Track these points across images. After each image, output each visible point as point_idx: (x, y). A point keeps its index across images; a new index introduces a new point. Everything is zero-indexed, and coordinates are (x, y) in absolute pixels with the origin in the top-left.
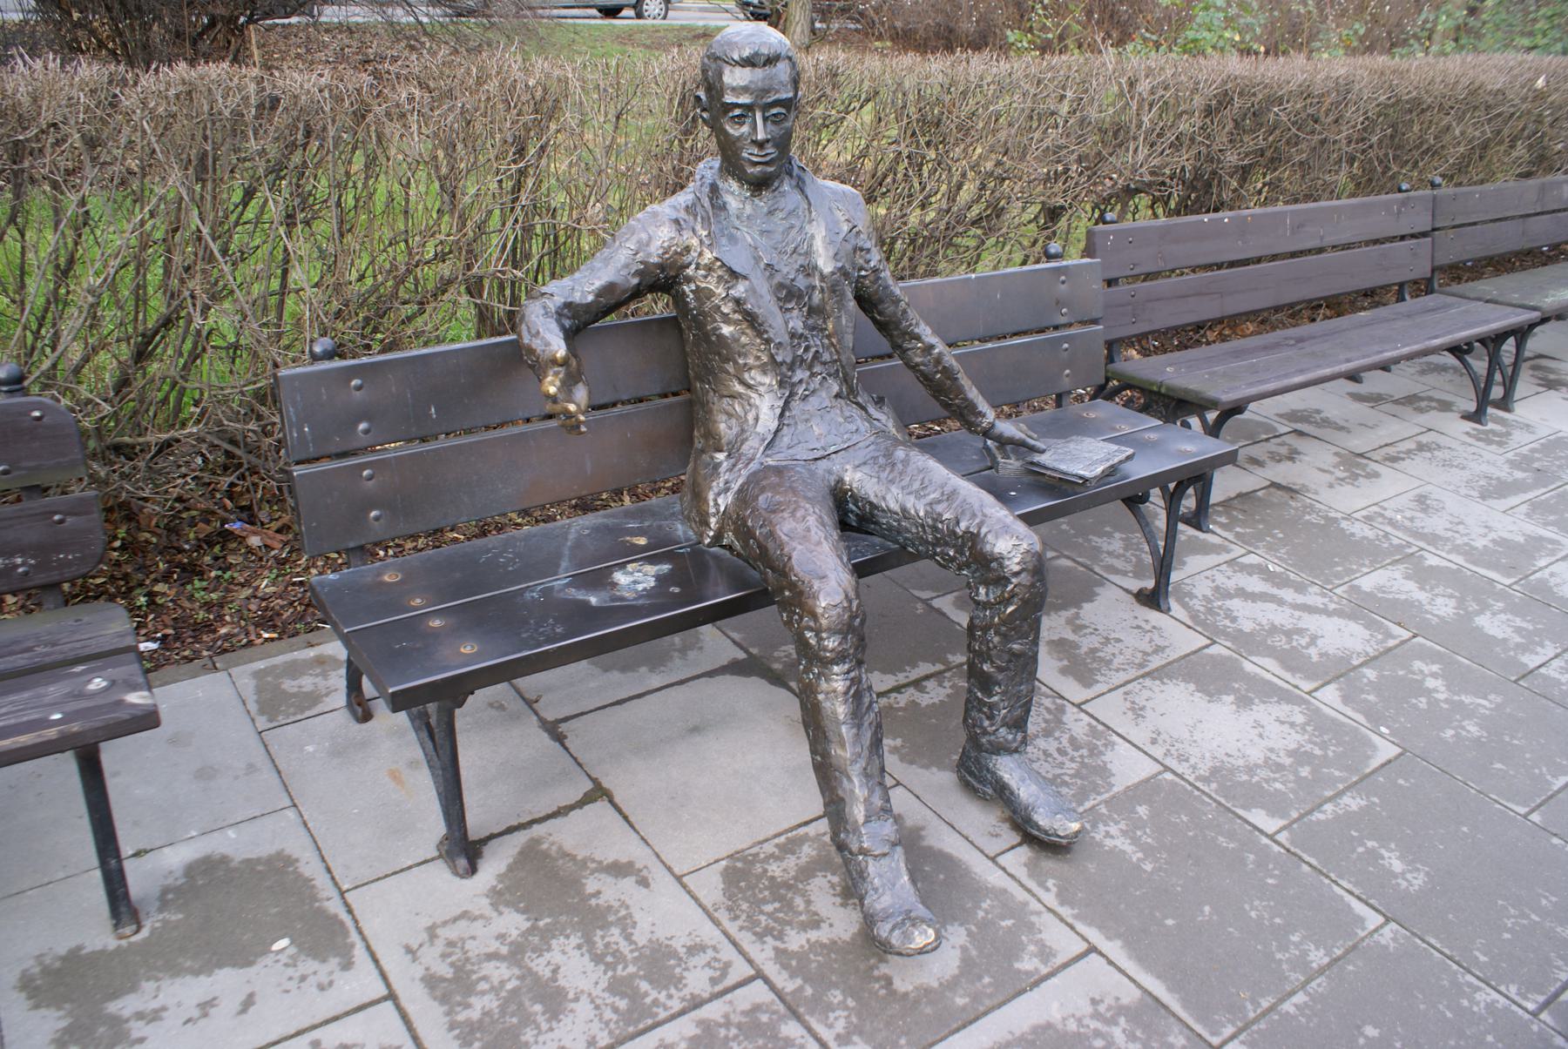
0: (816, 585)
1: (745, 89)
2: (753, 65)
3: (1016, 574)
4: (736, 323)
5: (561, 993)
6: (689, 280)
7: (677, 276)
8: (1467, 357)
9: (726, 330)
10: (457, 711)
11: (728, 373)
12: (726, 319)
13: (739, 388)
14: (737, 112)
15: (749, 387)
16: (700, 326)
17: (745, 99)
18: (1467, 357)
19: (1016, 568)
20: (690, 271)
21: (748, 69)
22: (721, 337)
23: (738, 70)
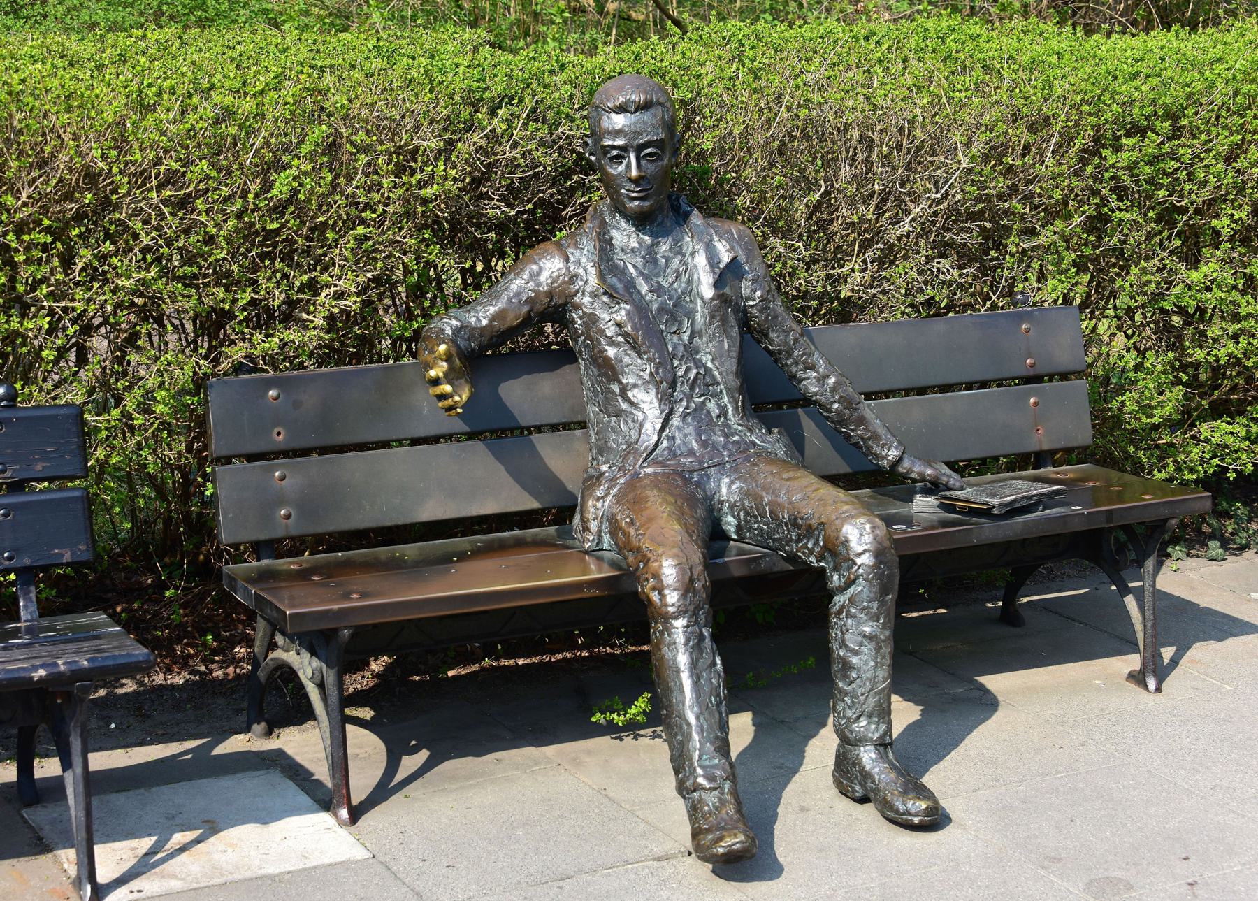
6: (577, 307)
7: (566, 304)
9: (611, 352)
11: (613, 392)
12: (612, 343)
13: (624, 406)
14: (615, 153)
15: (632, 404)
19: (860, 549)
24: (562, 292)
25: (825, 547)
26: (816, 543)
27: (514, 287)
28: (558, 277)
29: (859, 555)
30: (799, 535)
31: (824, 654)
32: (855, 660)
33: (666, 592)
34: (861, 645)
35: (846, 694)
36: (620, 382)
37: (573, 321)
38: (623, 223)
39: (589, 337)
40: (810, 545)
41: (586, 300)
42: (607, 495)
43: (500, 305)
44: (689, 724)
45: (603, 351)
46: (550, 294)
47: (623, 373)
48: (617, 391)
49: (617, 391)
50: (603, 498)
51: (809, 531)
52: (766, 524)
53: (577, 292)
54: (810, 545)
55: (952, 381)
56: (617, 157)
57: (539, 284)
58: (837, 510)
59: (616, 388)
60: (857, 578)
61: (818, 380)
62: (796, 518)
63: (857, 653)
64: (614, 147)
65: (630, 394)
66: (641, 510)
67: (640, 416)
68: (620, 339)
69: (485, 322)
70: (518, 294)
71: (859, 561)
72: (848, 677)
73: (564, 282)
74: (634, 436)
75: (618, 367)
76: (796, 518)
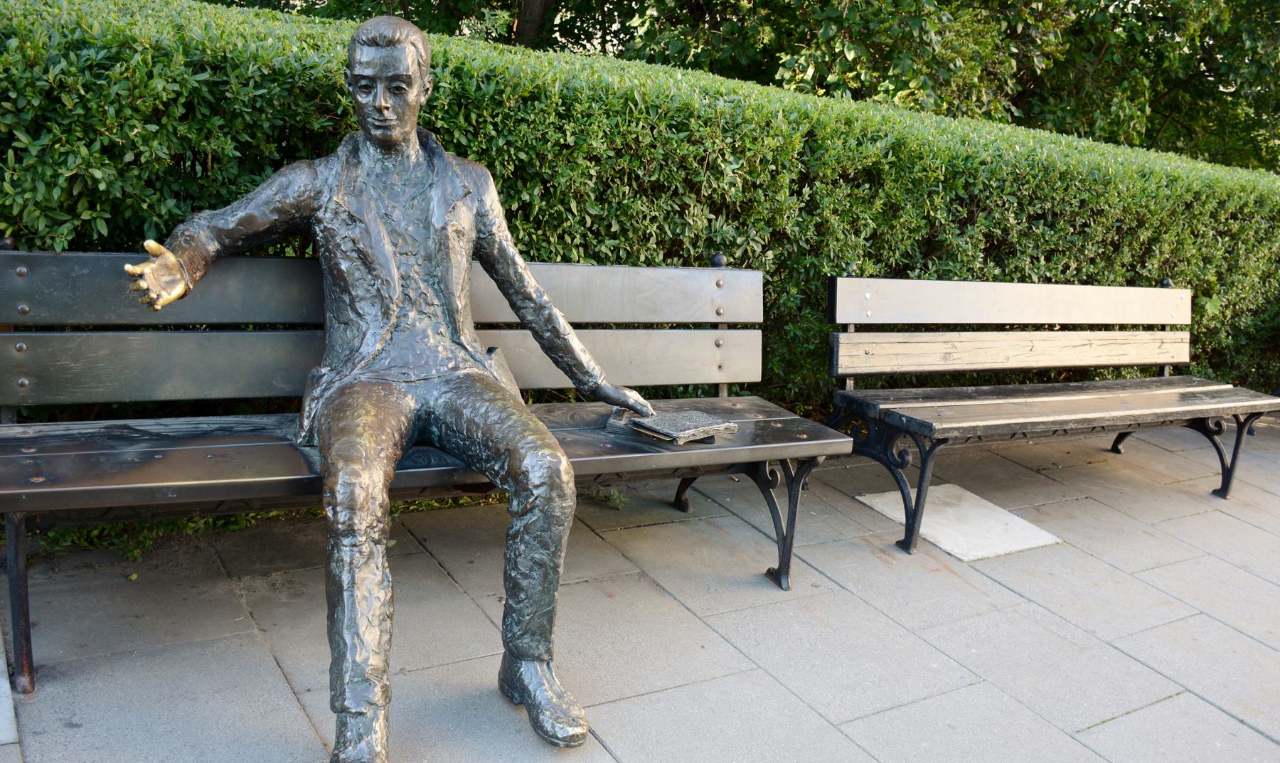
0: (341, 464)
1: (368, 64)
2: (377, 45)
3: (537, 487)
4: (351, 260)
5: (409, 77)
6: (319, 221)
7: (310, 217)
8: (1216, 438)
9: (344, 266)
10: (776, 566)
11: (344, 302)
12: (347, 258)
13: (352, 315)
14: (363, 82)
15: (359, 315)
16: (329, 259)
17: (368, 72)
18: (1216, 438)
19: (537, 482)
20: (320, 214)
21: (373, 49)
22: (340, 270)
23: (365, 48)
24: (308, 205)
25: (508, 472)
26: (502, 467)
27: (263, 196)
28: (304, 193)
29: (537, 487)
30: (488, 456)
31: (576, 483)
32: (524, 583)
33: (339, 509)
34: (531, 570)
35: (515, 611)
36: (350, 294)
37: (316, 234)
38: (372, 150)
39: (327, 250)
40: (496, 468)
41: (328, 215)
42: (321, 396)
43: (248, 211)
44: (345, 643)
45: (337, 264)
46: (297, 207)
47: (354, 286)
48: (347, 300)
49: (347, 300)
50: (318, 398)
51: (497, 455)
52: (464, 440)
53: (321, 207)
54: (496, 468)
55: (240, 320)
56: (366, 87)
57: (287, 196)
58: (524, 437)
59: (347, 299)
60: (534, 507)
61: (535, 310)
62: (487, 440)
63: (525, 576)
64: (363, 77)
65: (358, 305)
66: (339, 419)
67: (364, 326)
68: (354, 255)
69: (232, 226)
70: (267, 203)
71: (536, 492)
72: (517, 596)
73: (310, 197)
74: (357, 344)
75: (350, 280)
76: (487, 440)
